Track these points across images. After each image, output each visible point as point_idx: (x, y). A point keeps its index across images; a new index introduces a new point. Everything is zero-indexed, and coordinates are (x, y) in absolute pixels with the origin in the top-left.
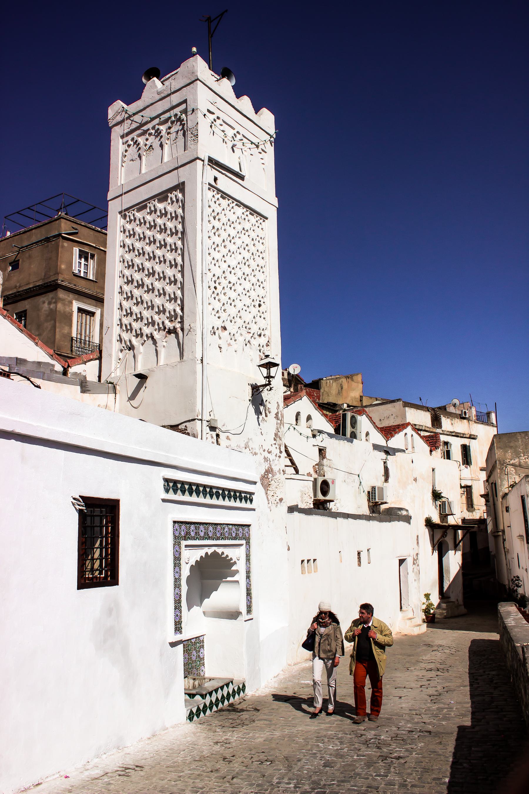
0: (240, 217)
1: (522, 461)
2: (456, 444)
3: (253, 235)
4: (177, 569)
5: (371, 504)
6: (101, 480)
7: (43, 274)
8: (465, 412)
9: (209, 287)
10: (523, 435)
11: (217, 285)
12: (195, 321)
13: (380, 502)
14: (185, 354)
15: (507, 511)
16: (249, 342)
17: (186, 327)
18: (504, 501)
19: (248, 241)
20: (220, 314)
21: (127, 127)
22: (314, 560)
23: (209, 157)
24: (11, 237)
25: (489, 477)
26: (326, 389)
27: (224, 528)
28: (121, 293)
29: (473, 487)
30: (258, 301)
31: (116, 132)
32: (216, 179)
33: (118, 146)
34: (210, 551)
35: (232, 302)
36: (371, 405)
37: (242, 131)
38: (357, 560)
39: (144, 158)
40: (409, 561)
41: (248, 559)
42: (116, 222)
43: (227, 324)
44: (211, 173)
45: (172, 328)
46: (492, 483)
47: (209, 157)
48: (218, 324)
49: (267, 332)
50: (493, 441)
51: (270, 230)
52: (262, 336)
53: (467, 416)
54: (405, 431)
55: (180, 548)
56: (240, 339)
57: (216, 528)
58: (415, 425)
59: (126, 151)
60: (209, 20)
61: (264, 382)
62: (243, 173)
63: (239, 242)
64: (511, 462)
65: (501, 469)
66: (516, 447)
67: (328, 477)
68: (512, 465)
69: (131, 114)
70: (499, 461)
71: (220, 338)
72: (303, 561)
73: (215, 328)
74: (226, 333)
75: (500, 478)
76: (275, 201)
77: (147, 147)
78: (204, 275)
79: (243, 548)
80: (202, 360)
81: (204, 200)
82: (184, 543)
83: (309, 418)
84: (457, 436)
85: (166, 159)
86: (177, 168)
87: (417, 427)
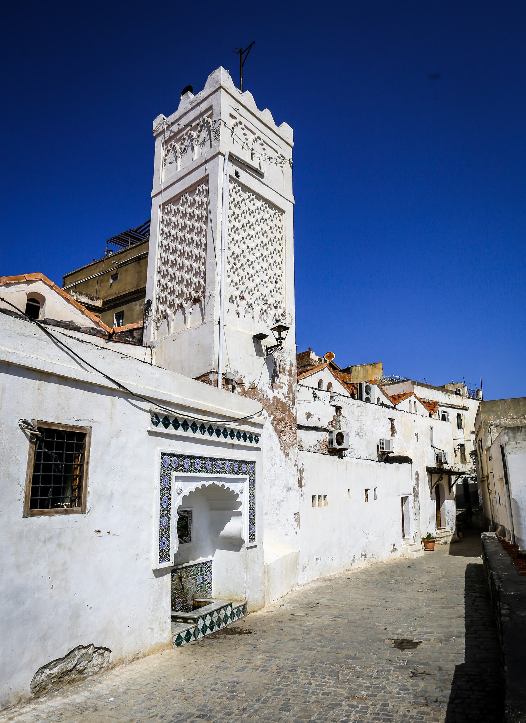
0: (259, 208)
1: (502, 422)
2: (452, 414)
3: (272, 224)
4: (165, 498)
5: (380, 453)
6: (62, 408)
7: (136, 283)
8: (459, 390)
9: (229, 262)
10: (503, 402)
11: (237, 261)
12: (213, 289)
13: (387, 451)
14: (205, 317)
15: (490, 460)
16: (265, 311)
17: (207, 294)
18: (488, 453)
19: (267, 228)
20: (239, 286)
21: (167, 135)
22: (325, 496)
23: (230, 152)
24: (112, 257)
25: (477, 436)
26: (356, 373)
27: (225, 463)
28: (160, 272)
29: (466, 445)
30: (275, 278)
31: (158, 142)
32: (237, 173)
33: (160, 152)
34: (207, 484)
35: (251, 277)
36: (387, 384)
37: (262, 137)
38: (364, 496)
39: (179, 159)
40: (411, 498)
41: (252, 491)
42: (157, 215)
43: (246, 295)
44: (231, 169)
45: (196, 297)
46: (479, 440)
47: (230, 152)
48: (237, 293)
49: (283, 305)
50: (479, 407)
51: (288, 221)
52: (278, 307)
53: (461, 393)
54: (409, 398)
55: (170, 479)
56: (257, 309)
57: (215, 463)
58: (421, 398)
59: (166, 155)
60: (241, 52)
61: (275, 343)
62: (262, 171)
63: (258, 229)
64: (493, 423)
65: (486, 428)
66: (497, 411)
67: (344, 430)
68: (496, 426)
69: (169, 123)
70: (484, 422)
71: (238, 306)
72: (313, 497)
73: (234, 298)
74: (244, 302)
75: (485, 435)
76: (292, 199)
77: (182, 150)
78: (223, 251)
79: (247, 483)
80: (219, 322)
81: (224, 189)
82: (174, 474)
83: (330, 385)
84: (453, 408)
85: (195, 158)
86: (204, 164)
87: (423, 400)
